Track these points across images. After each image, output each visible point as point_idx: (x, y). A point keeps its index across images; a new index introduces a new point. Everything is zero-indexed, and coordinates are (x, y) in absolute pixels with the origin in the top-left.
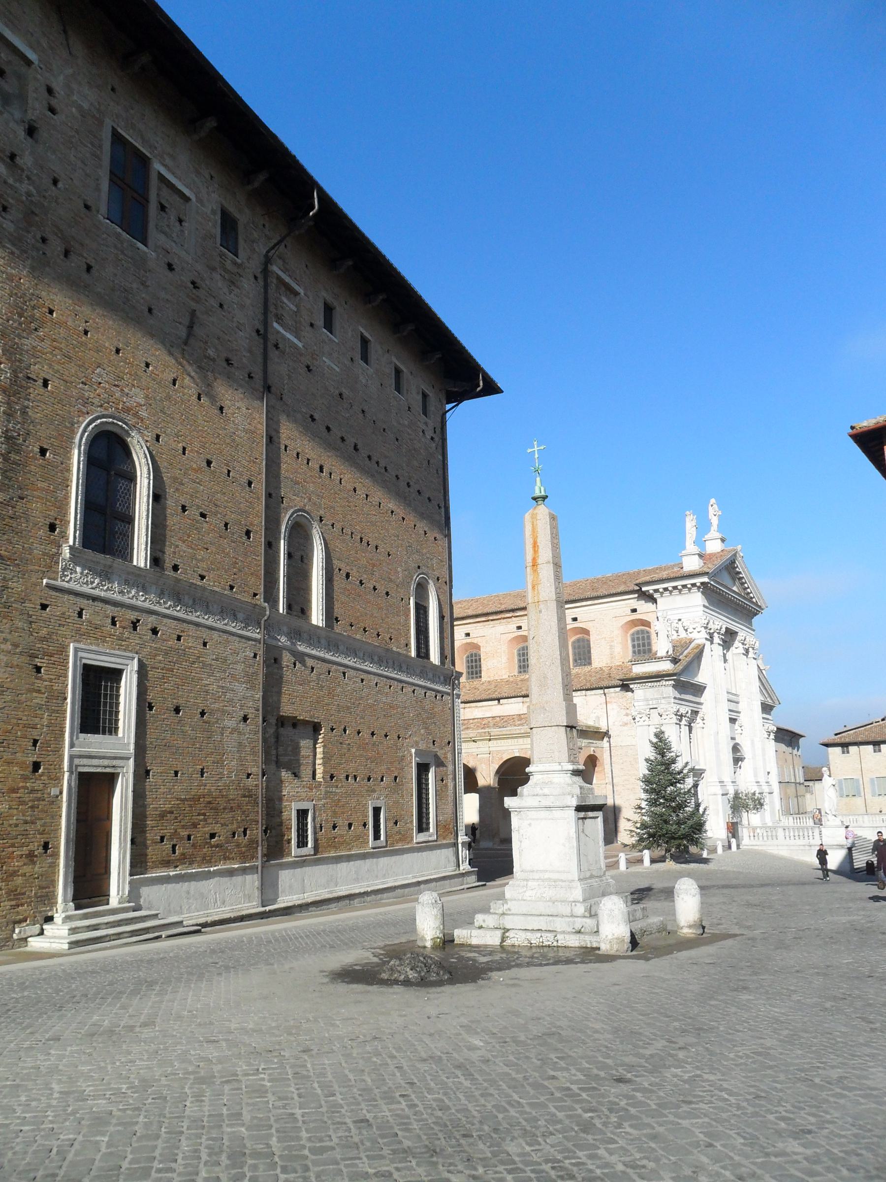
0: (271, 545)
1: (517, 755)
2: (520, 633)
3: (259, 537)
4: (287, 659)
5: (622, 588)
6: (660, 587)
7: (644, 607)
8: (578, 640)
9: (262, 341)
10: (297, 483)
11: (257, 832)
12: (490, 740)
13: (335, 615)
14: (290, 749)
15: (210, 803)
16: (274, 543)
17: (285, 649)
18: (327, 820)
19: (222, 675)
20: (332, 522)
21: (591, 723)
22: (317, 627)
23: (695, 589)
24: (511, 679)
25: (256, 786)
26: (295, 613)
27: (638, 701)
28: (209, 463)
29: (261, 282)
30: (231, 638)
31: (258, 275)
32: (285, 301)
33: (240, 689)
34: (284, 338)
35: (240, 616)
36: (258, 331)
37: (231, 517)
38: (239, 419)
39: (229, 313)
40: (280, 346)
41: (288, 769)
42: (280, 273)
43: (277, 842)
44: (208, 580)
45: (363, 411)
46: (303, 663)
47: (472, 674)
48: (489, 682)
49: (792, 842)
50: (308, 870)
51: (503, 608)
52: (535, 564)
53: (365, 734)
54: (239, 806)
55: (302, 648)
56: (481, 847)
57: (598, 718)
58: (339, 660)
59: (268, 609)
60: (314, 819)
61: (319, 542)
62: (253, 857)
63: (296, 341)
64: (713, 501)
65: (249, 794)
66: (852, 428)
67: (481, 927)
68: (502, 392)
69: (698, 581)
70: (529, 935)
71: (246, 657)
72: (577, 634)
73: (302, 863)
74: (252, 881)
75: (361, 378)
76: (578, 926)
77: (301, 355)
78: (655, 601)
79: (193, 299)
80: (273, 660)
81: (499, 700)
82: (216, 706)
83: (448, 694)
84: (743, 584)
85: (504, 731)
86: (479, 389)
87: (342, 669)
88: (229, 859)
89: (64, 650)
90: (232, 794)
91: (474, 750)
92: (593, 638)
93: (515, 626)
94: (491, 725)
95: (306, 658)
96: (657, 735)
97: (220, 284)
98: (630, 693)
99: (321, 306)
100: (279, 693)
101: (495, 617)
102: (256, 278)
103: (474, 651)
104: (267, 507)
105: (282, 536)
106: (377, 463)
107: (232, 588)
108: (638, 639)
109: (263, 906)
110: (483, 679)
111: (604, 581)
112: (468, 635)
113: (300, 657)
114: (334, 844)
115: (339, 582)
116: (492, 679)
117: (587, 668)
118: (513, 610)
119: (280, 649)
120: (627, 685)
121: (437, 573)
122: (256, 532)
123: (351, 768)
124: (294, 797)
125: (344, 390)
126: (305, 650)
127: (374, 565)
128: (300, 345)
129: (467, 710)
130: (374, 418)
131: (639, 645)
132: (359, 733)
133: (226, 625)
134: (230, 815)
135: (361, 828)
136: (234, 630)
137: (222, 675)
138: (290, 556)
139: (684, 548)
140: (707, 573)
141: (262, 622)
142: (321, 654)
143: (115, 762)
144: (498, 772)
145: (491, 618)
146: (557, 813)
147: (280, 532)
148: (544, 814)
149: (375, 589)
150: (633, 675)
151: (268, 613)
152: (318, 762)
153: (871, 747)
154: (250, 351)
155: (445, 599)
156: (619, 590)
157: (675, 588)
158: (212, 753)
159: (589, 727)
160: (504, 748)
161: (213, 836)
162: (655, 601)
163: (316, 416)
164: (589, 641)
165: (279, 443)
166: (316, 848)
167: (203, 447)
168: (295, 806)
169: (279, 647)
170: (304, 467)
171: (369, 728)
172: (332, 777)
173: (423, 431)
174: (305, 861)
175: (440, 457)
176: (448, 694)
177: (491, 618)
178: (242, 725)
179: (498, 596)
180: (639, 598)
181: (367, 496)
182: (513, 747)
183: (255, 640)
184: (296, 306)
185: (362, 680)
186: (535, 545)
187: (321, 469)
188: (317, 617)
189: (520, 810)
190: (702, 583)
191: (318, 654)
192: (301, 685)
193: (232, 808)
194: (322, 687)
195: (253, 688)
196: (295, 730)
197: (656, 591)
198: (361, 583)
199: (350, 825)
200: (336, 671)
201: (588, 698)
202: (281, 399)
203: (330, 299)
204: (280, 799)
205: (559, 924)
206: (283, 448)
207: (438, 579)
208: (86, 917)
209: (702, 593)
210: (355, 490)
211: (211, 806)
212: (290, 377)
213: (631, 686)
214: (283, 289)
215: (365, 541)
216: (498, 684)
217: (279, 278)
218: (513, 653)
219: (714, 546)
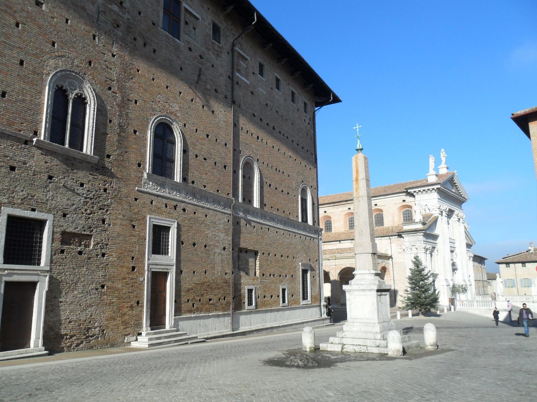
0: (235, 172)
1: (349, 266)
3: (230, 169)
4: (243, 222)
5: (398, 191)
6: (417, 190)
7: (409, 199)
10: (247, 144)
11: (230, 298)
15: (209, 285)
18: (261, 294)
22: (256, 208)
23: (434, 191)
27: (406, 242)
28: (208, 136)
32: (242, 63)
33: (222, 235)
34: (241, 79)
35: (222, 203)
37: (218, 160)
42: (239, 50)
46: (250, 224)
49: (481, 307)
50: (253, 316)
51: (342, 200)
52: (357, 180)
53: (278, 256)
55: (249, 218)
57: (387, 250)
58: (266, 223)
60: (255, 293)
63: (246, 81)
64: (443, 150)
65: (226, 282)
66: (513, 115)
67: (332, 343)
69: (435, 187)
70: (355, 347)
73: (250, 312)
76: (378, 344)
77: (249, 87)
78: (414, 196)
79: (200, 63)
80: (236, 223)
81: (340, 241)
83: (316, 238)
84: (457, 188)
87: (268, 227)
89: (144, 218)
90: (219, 281)
96: (415, 258)
98: (402, 239)
99: (258, 64)
102: (228, 53)
103: (328, 219)
106: (284, 135)
107: (218, 191)
108: (406, 214)
110: (333, 232)
111: (390, 188)
112: (325, 212)
114: (264, 304)
117: (381, 227)
118: (346, 201)
119: (240, 218)
120: (401, 235)
121: (311, 184)
122: (229, 166)
125: (268, 102)
128: (248, 82)
131: (406, 217)
138: (244, 177)
139: (429, 172)
140: (439, 184)
142: (258, 221)
143: (167, 267)
144: (339, 274)
146: (368, 293)
148: (362, 293)
149: (282, 191)
152: (257, 268)
153: (520, 265)
154: (226, 86)
157: (424, 190)
161: (210, 300)
162: (414, 196)
163: (256, 114)
164: (382, 215)
172: (263, 275)
175: (313, 132)
176: (316, 238)
178: (223, 251)
180: (406, 195)
186: (357, 171)
188: (256, 204)
189: (350, 291)
190: (437, 188)
195: (227, 235)
197: (415, 192)
198: (276, 189)
199: (272, 296)
200: (265, 228)
204: (240, 284)
205: (368, 343)
208: (155, 334)
209: (437, 193)
210: (273, 147)
215: (278, 170)
216: (339, 234)
217: (239, 53)
219: (443, 171)
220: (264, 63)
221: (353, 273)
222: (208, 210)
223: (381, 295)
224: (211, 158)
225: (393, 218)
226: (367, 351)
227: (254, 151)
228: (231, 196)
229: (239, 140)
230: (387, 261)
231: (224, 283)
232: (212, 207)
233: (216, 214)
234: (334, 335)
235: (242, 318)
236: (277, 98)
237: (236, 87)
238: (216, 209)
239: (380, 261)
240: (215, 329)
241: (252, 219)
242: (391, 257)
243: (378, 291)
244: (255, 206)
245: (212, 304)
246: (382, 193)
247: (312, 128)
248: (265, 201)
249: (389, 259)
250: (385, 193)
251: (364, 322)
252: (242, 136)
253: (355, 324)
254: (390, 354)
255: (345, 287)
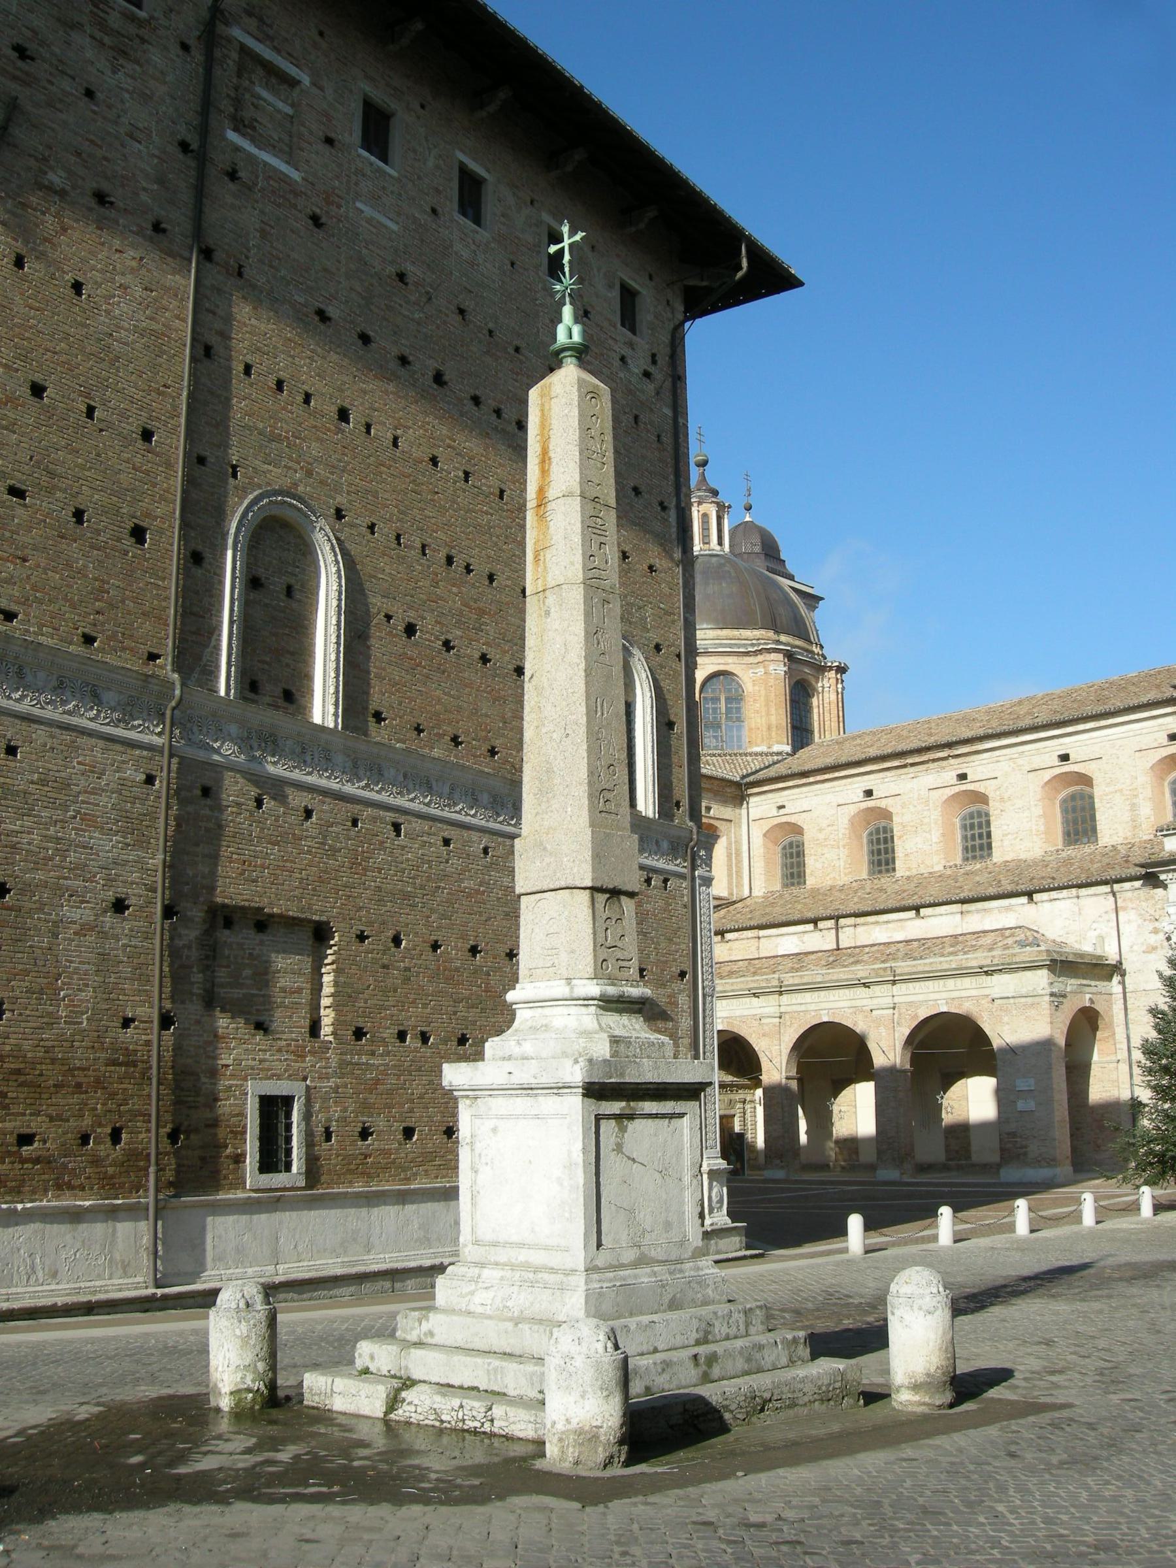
0: (198, 560)
1: (944, 1009)
2: (964, 788)
3: (168, 543)
4: (234, 790)
5: (1152, 696)
8: (1073, 797)
9: (193, 164)
10: (276, 439)
11: (148, 1136)
12: (894, 982)
13: (373, 706)
14: (247, 972)
15: (18, 1072)
16: (207, 555)
17: (232, 770)
18: (343, 1120)
19: (58, 815)
20: (368, 521)
21: (1087, 948)
22: (322, 728)
24: (949, 872)
25: (148, 1043)
26: (267, 699)
28: (37, 390)
29: (198, 55)
30: (82, 741)
31: (192, 42)
32: (265, 94)
33: (107, 845)
34: (251, 159)
35: (110, 697)
36: (184, 146)
37: (90, 499)
38: (122, 308)
39: (110, 107)
40: (241, 174)
41: (236, 1009)
42: (250, 42)
43: (203, 1159)
44: (22, 622)
45: (462, 312)
46: (280, 798)
47: (880, 864)
48: (908, 878)
50: (288, 1219)
51: (931, 741)
53: (454, 950)
54: (99, 1083)
55: (275, 768)
56: (1003, 1180)
57: (1102, 938)
58: (383, 797)
59: (178, 686)
60: (307, 1116)
61: (330, 558)
62: (137, 1187)
63: (284, 167)
65: (128, 1060)
68: (801, 284)
71: (122, 782)
72: (1071, 785)
73: (274, 1202)
74: (132, 1236)
75: (458, 247)
77: (296, 194)
79: (15, 78)
80: (198, 791)
81: (917, 909)
82: (40, 876)
83: (682, 876)
85: (922, 965)
86: (740, 274)
87: (390, 816)
88: (71, 1187)
90: (80, 1056)
91: (865, 1002)
92: (1098, 791)
93: (954, 774)
94: (900, 955)
95: (289, 791)
97: (89, 54)
98: (1160, 891)
99: (356, 109)
100: (214, 858)
101: (917, 759)
102: (185, 47)
103: (883, 823)
104: (190, 482)
105: (230, 541)
106: (498, 412)
107: (89, 640)
109: (158, 1287)
110: (898, 874)
111: (1122, 686)
112: (869, 793)
113: (277, 788)
114: (360, 1168)
115: (383, 645)
116: (914, 872)
117: (1088, 849)
118: (950, 745)
119: (217, 769)
121: (654, 637)
122: (161, 531)
123: (413, 1018)
124: (249, 1070)
125: (409, 268)
126: (287, 774)
127: (482, 612)
128: (296, 175)
129: (860, 929)
130: (491, 325)
132: (435, 946)
133: (69, 713)
134: (76, 1099)
135: (439, 1138)
136: (92, 725)
137: (58, 815)
138: (253, 583)
141: (168, 713)
142: (334, 785)
144: (910, 1041)
145: (910, 761)
146: (549, 1104)
147: (225, 536)
148: (521, 1104)
149: (484, 659)
150: (1164, 855)
151: (178, 692)
152: (325, 1001)
154: (161, 181)
155: (675, 690)
156: (1144, 699)
158: (27, 972)
159: (1082, 955)
160: (921, 998)
161: (25, 1139)
163: (332, 311)
164: (1091, 797)
165: (229, 359)
166: (312, 1174)
167: (25, 358)
168: (254, 1090)
169: (214, 766)
170: (298, 409)
171: (464, 937)
172: (359, 1034)
173: (623, 359)
174: (279, 1199)
175: (668, 412)
176: (682, 876)
177: (910, 761)
178: (109, 919)
179: (929, 722)
181: (467, 474)
182: (936, 996)
183: (150, 748)
184: (292, 105)
185: (447, 842)
187: (343, 415)
188: (323, 707)
189: (476, 1093)
191: (323, 782)
192: (276, 843)
193: (79, 1085)
194: (335, 851)
195: (142, 843)
196: (261, 936)
198: (448, 646)
199: (408, 1132)
200: (374, 819)
201: (1082, 901)
202: (240, 274)
203: (380, 96)
204: (214, 1073)
206: (241, 368)
207: (658, 648)
210: (434, 461)
211: (22, 1078)
212: (264, 234)
213: (1163, 877)
214: (260, 72)
215: (459, 562)
216: (922, 881)
217: (244, 50)
218: (953, 824)
220: (393, 105)
221: (511, 996)
222: (25, 725)
223: (631, 1117)
224: (50, 490)
225: (1134, 807)
226: (487, 1427)
227: (319, 469)
228: (166, 667)
229: (226, 419)
230: (1102, 985)
231: (114, 1063)
232: (49, 713)
233: (73, 747)
234: (386, 1333)
235: (222, 1231)
236: (465, 254)
237: (224, 191)
238: (75, 720)
239: (1071, 984)
240: (54, 1275)
241: (296, 775)
242: (1115, 970)
243: (595, 1091)
244: (317, 719)
245: (37, 1161)
246: (1089, 710)
247: (667, 395)
248: (378, 698)
249: (1109, 978)
250: (1100, 709)
251: (526, 1266)
252: (246, 403)
253: (486, 1273)
254: (556, 1456)
255: (454, 1075)
